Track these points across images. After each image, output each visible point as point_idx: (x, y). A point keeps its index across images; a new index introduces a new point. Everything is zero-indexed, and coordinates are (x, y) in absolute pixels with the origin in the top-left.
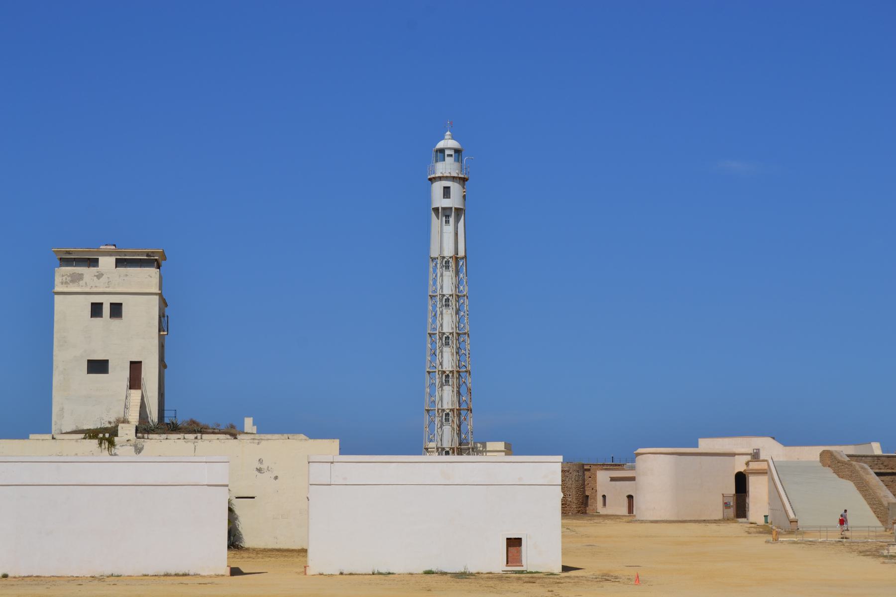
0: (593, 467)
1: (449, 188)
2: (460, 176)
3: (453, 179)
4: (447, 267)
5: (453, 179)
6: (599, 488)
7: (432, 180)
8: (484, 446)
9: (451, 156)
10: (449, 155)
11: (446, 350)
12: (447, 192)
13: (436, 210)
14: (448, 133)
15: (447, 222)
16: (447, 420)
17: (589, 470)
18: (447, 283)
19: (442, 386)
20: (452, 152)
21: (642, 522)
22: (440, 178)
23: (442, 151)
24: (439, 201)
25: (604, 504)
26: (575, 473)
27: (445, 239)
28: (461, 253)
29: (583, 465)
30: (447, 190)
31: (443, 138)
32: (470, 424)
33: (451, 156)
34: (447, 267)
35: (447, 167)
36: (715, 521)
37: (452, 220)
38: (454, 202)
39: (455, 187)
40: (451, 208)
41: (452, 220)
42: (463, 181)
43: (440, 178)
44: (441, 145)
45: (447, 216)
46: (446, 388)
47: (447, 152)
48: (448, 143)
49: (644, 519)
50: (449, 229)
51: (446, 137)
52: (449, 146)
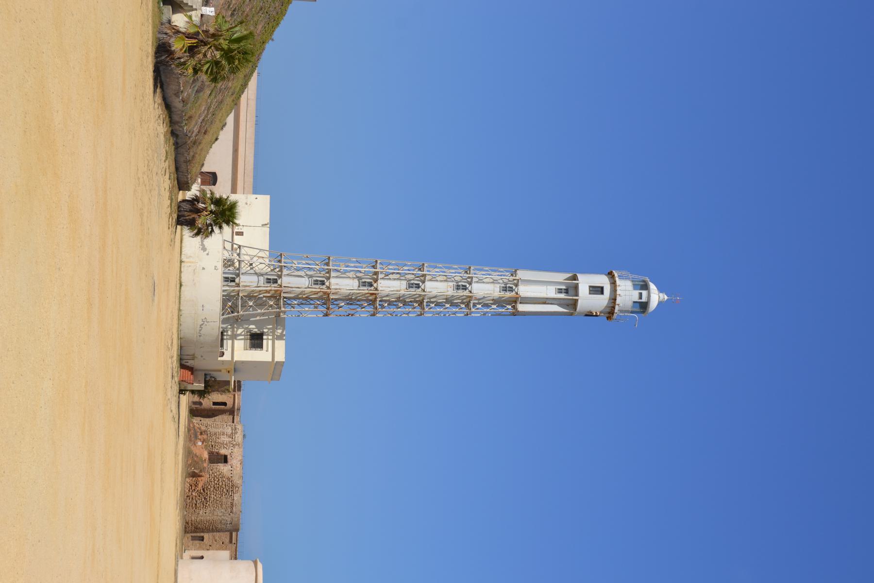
0: (234, 547)
1: (602, 293)
2: (617, 308)
3: (613, 299)
4: (505, 289)
5: (613, 299)
6: (211, 552)
7: (610, 275)
8: (280, 338)
9: (641, 297)
10: (641, 294)
11: (404, 284)
12: (597, 290)
13: (575, 278)
14: (666, 297)
15: (560, 291)
16: (316, 282)
17: (231, 542)
18: (486, 287)
19: (359, 278)
20: (644, 299)
21: (177, 564)
22: (613, 284)
23: (645, 287)
24: (585, 282)
25: (193, 558)
26: (229, 520)
27: (539, 287)
28: (521, 308)
29: (237, 530)
30: (599, 290)
31: (661, 290)
32: (310, 313)
33: (641, 297)
34: (505, 289)
35: (627, 293)
36: (179, 324)
37: (562, 296)
38: (587, 301)
39: (600, 302)
40: (577, 295)
41: (562, 296)
42: (610, 312)
43: (613, 284)
44: (652, 286)
45: (567, 291)
46: (356, 283)
47: (644, 293)
48: (655, 297)
49: (179, 565)
50: (550, 292)
51: (661, 295)
52: (652, 295)
